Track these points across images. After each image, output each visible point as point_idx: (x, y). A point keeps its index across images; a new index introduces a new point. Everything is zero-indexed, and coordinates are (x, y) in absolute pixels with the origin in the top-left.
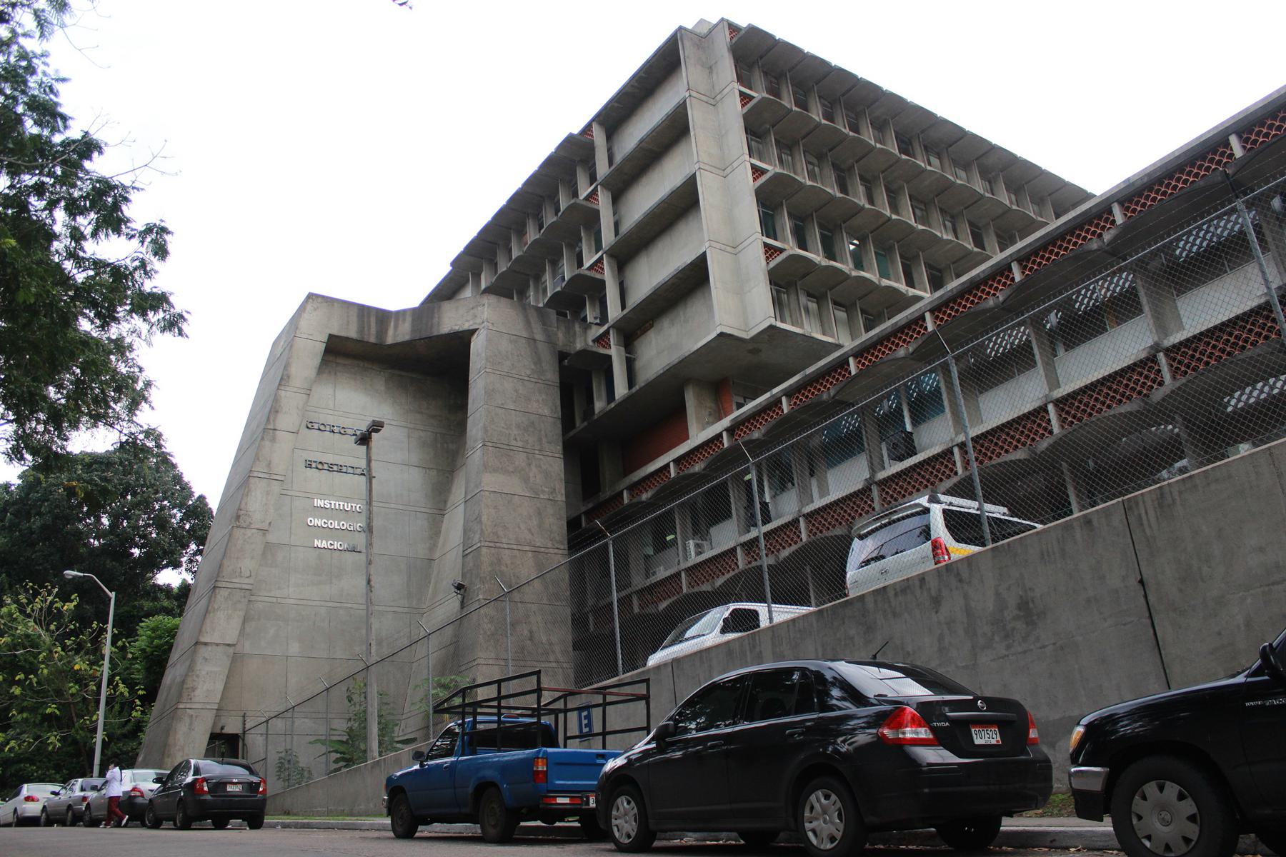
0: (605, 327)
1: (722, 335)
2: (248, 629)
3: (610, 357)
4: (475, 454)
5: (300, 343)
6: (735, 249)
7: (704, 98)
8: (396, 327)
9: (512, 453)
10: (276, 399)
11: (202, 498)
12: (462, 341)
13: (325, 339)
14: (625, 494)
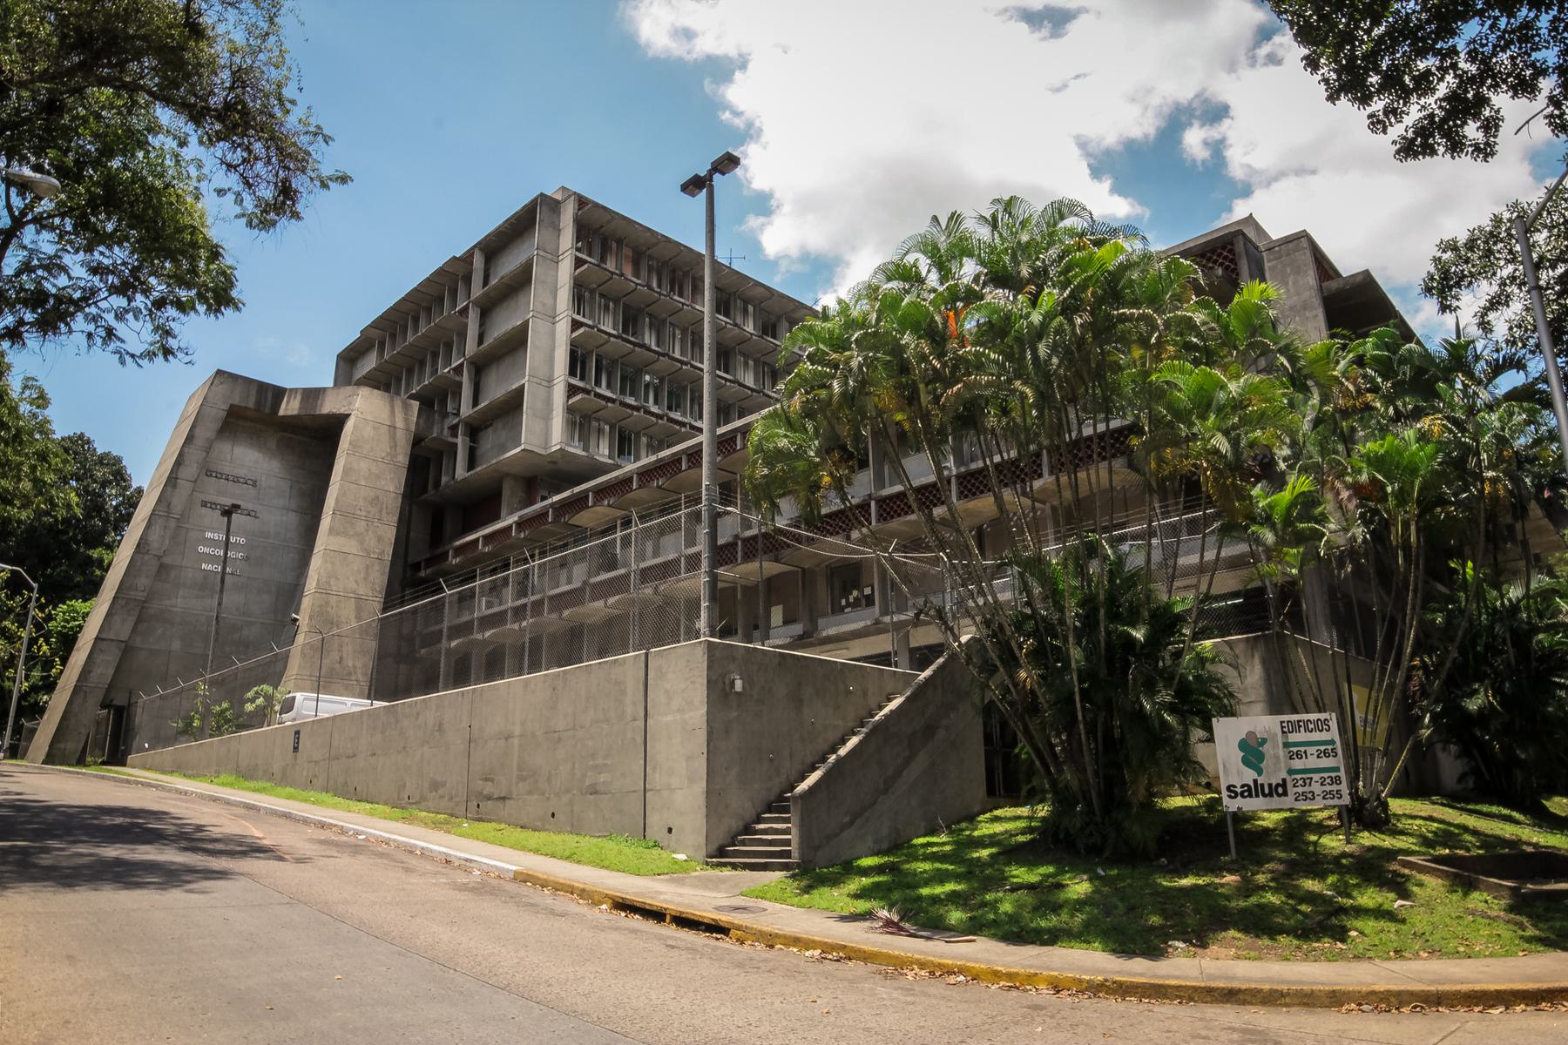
13: (226, 407)
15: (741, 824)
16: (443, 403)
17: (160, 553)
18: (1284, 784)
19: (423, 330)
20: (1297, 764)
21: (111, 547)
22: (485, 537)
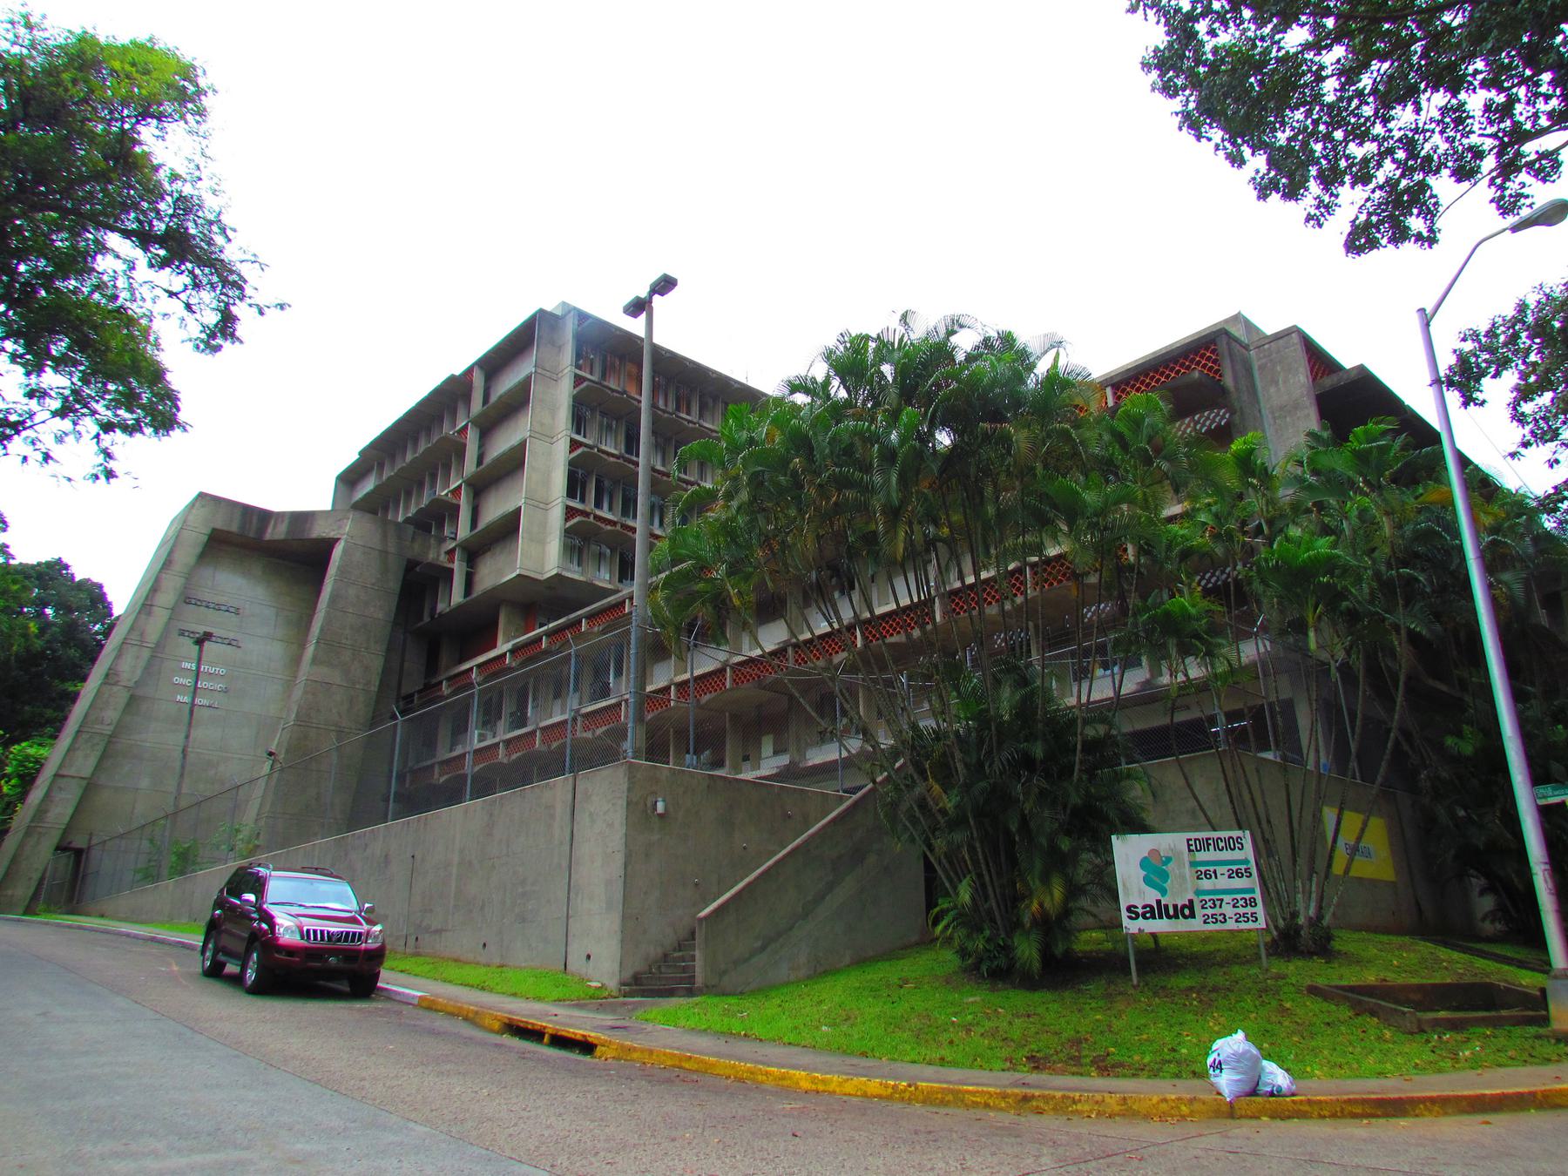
6: (545, 506)
12: (330, 544)
13: (208, 531)
15: (660, 951)
16: (441, 526)
17: (131, 684)
18: (1191, 904)
19: (421, 448)
20: (1206, 884)
21: (84, 679)
22: (479, 666)
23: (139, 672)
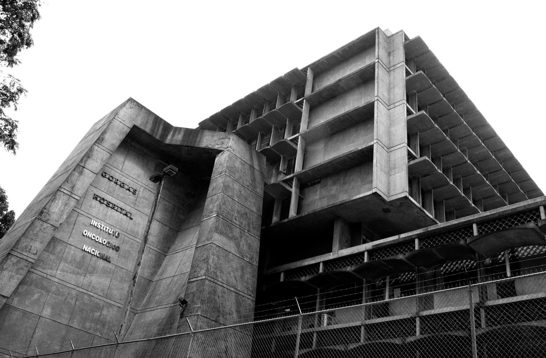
0: (292, 175)
1: (375, 194)
2: (20, 290)
3: (291, 193)
4: (210, 218)
5: (116, 123)
6: (389, 149)
7: (384, 66)
8: (173, 135)
9: (232, 226)
10: (91, 150)
11: (12, 213)
13: (131, 126)
14: (282, 275)
23: (65, 217)
